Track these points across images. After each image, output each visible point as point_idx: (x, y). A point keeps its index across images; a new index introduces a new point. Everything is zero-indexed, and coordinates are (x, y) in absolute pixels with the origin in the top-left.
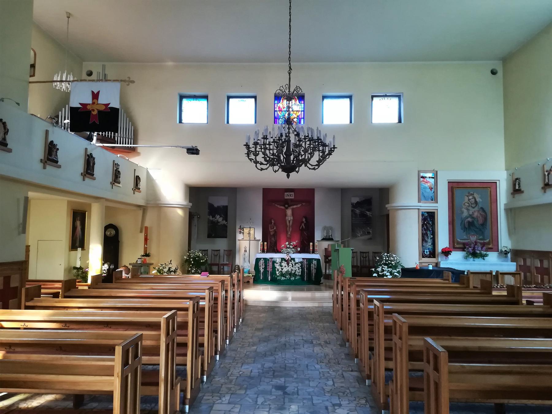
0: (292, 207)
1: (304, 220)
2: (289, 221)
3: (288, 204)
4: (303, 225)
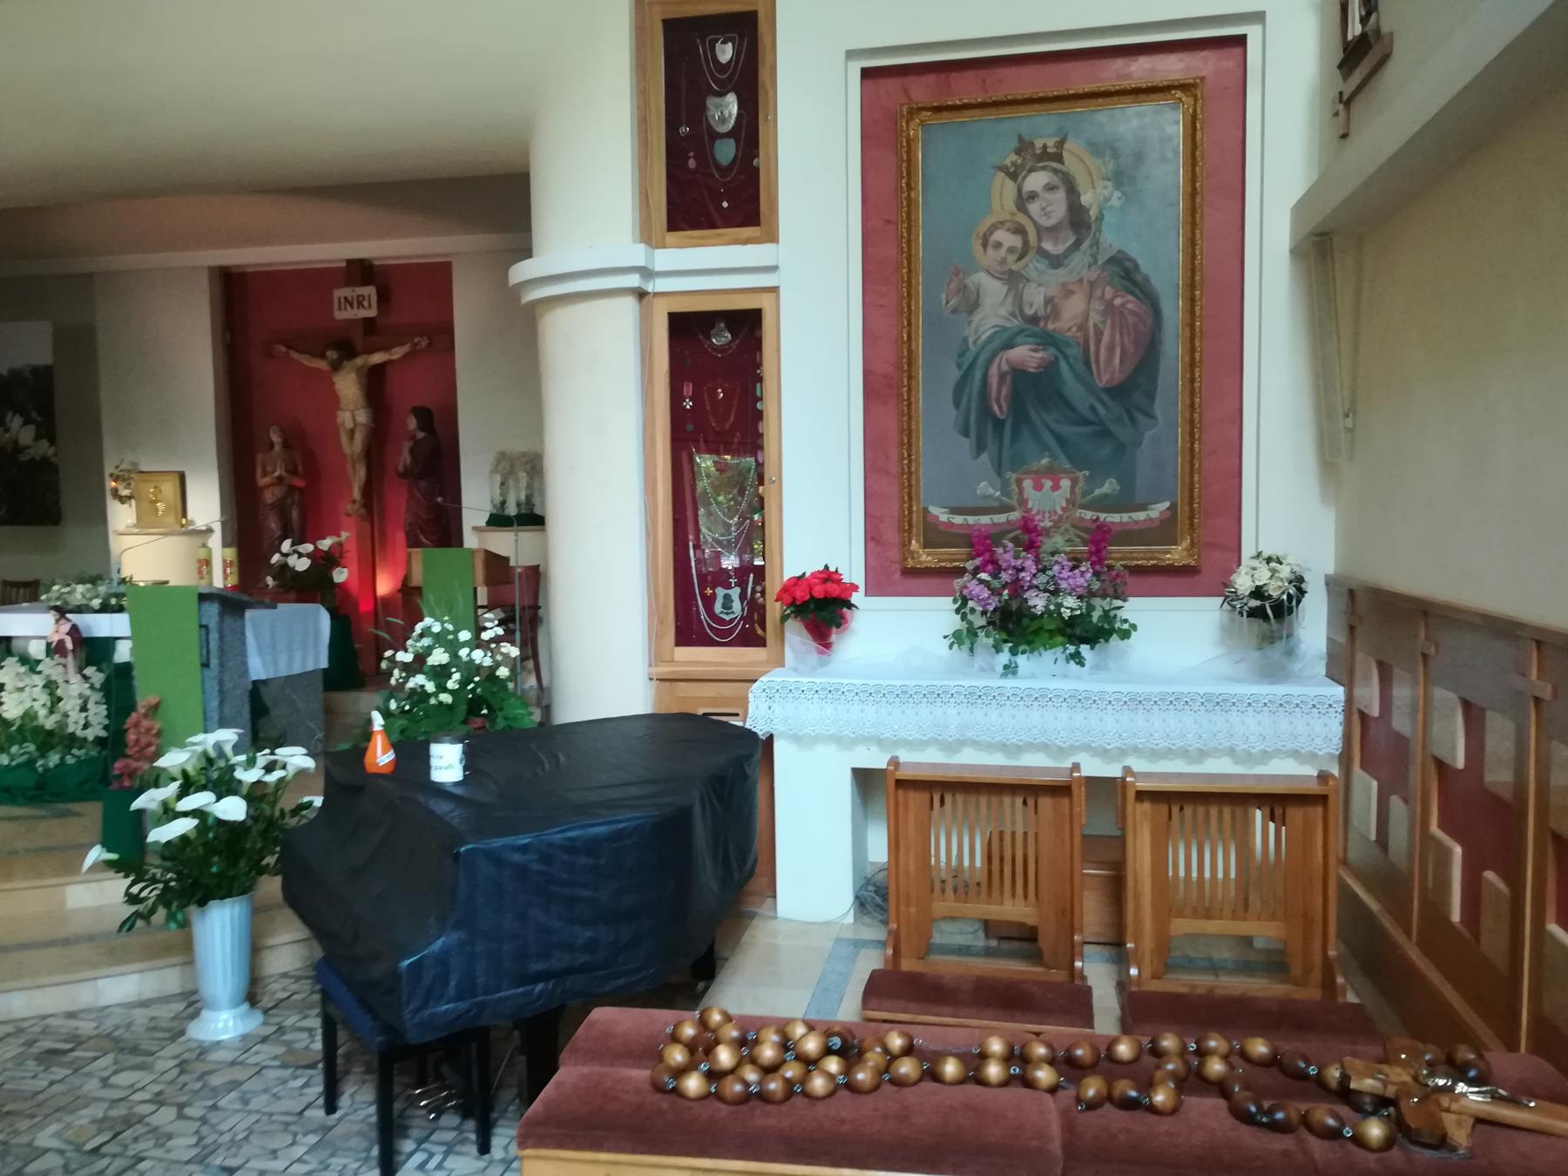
0: (359, 361)
2: (352, 433)
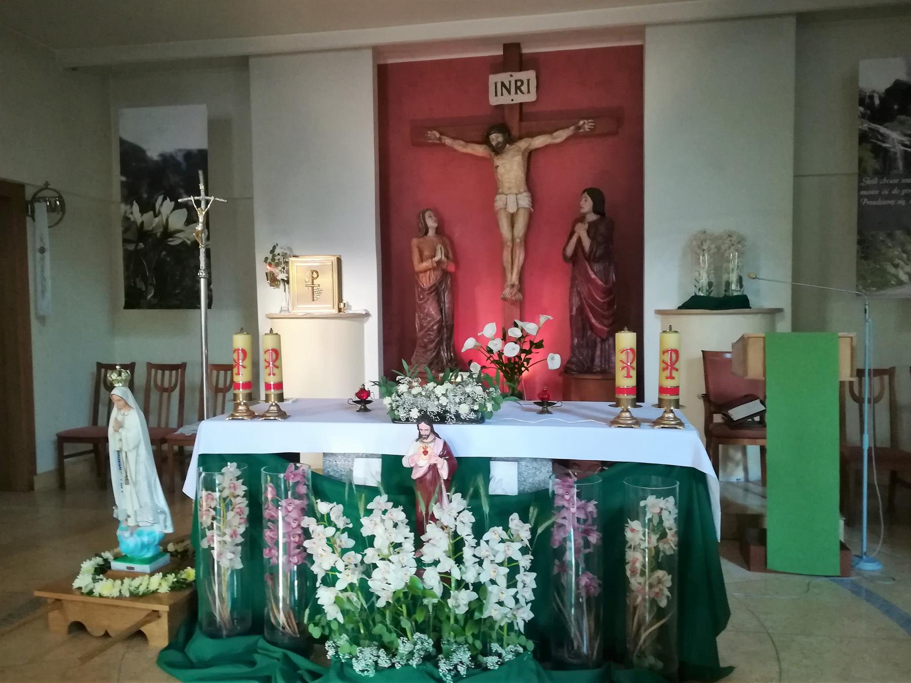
0: (523, 144)
1: (587, 205)
2: (512, 218)
3: (503, 128)
4: (581, 231)
